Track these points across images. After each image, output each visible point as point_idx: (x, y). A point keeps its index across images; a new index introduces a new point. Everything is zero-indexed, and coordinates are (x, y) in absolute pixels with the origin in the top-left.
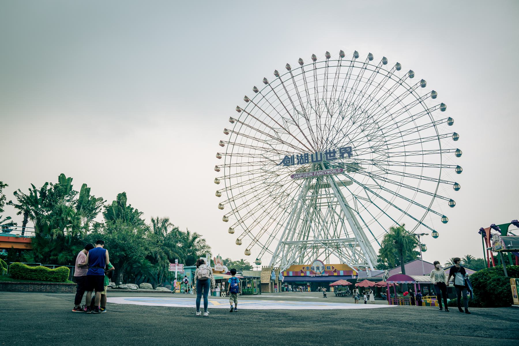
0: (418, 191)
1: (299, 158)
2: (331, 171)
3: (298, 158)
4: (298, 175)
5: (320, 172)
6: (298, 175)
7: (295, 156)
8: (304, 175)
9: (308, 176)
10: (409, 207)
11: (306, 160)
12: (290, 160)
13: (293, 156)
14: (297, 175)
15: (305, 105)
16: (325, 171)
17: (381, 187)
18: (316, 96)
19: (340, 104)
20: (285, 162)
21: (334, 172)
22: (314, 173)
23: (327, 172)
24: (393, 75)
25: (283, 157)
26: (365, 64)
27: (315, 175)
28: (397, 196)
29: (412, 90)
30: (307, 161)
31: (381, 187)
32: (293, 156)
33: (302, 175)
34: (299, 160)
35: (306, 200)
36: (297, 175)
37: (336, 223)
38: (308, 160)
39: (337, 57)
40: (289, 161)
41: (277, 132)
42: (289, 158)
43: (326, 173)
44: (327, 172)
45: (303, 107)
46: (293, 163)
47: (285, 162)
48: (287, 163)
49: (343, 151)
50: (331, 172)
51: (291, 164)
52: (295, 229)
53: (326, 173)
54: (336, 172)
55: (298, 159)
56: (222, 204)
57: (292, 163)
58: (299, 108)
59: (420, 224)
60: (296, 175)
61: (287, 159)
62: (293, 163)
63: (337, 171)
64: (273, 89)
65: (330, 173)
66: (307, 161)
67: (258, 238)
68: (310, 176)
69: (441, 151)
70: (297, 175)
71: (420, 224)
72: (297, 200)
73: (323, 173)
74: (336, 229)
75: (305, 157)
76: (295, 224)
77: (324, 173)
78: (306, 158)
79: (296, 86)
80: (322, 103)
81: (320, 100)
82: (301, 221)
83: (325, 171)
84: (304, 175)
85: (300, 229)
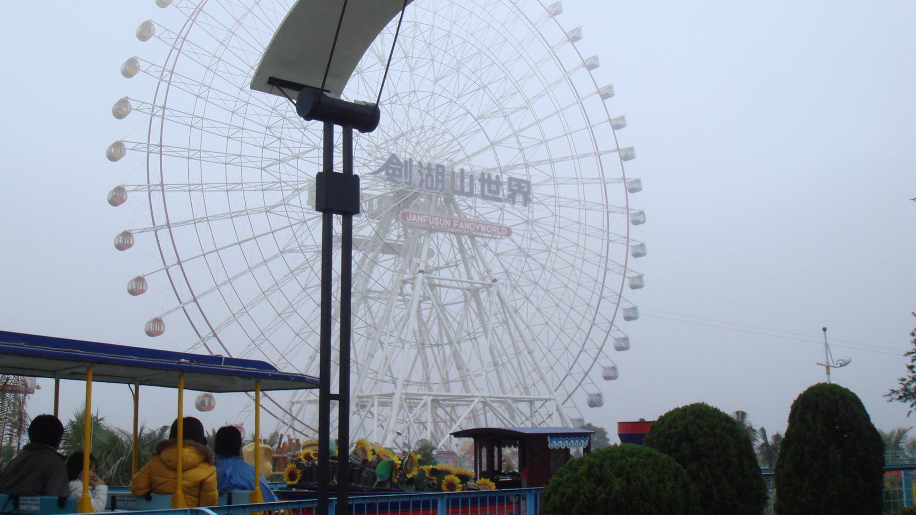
1: (425, 172)
3: (422, 170)
4: (466, 223)
5: (420, 215)
6: (419, 216)
7: (414, 163)
8: (431, 221)
12: (403, 169)
13: (411, 160)
14: (417, 215)
17: (287, 184)
18: (254, 189)
20: (391, 171)
21: (495, 230)
22: (455, 221)
24: (378, 136)
27: (457, 227)
30: (440, 187)
31: (287, 184)
32: (411, 160)
36: (415, 216)
40: (400, 170)
42: (399, 163)
46: (408, 180)
47: (391, 171)
48: (394, 174)
49: (514, 185)
51: (404, 180)
60: (413, 214)
61: (394, 164)
64: (280, 148)
65: (486, 230)
66: (440, 187)
68: (444, 226)
70: (415, 216)
73: (472, 227)
75: (438, 174)
77: (474, 228)
78: (440, 178)
80: (274, 173)
81: (267, 177)
84: (431, 221)
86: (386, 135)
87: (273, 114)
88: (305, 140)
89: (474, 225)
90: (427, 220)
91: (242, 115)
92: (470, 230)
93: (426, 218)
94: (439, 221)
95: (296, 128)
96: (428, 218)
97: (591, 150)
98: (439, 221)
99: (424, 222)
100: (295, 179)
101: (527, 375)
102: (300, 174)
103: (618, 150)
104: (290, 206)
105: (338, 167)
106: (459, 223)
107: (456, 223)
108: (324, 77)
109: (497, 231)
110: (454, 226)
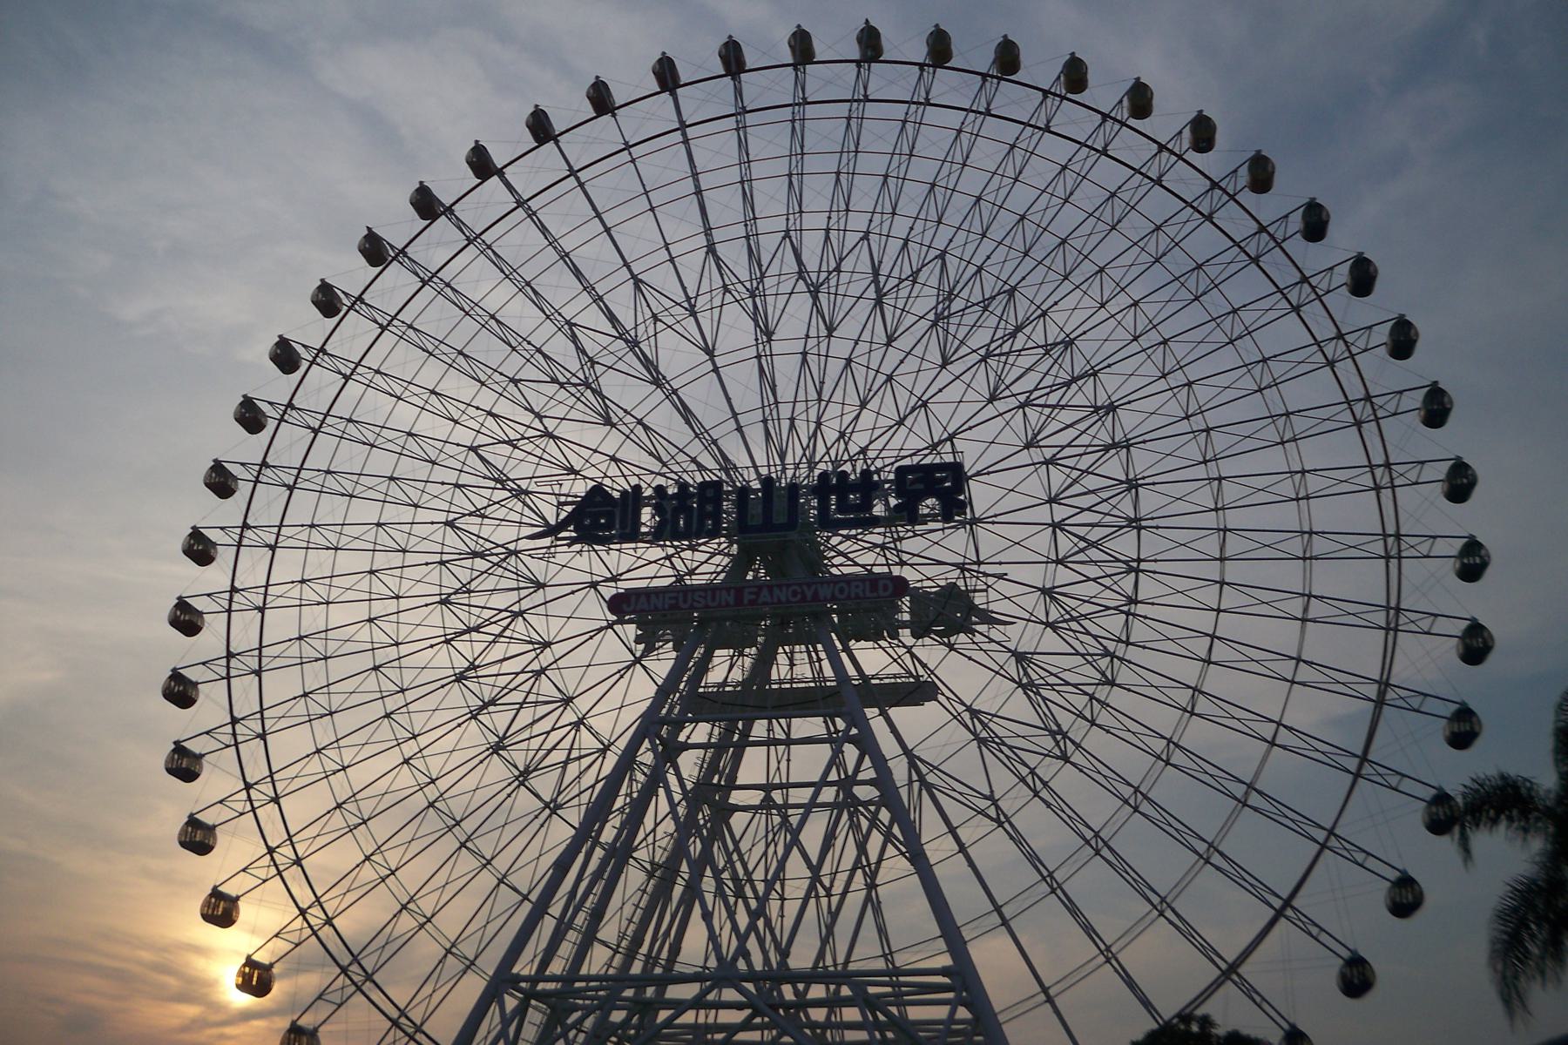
0: (1136, 809)
2: (838, 587)
3: (664, 503)
6: (653, 597)
8: (685, 601)
9: (707, 606)
10: (1185, 883)
11: (709, 516)
15: (768, 244)
16: (809, 585)
19: (1012, 320)
22: (747, 590)
23: (816, 589)
25: (581, 488)
26: (1109, 123)
27: (752, 603)
28: (1036, 794)
29: (1329, 349)
32: (637, 488)
33: (676, 598)
34: (668, 516)
35: (686, 746)
37: (835, 900)
38: (717, 515)
39: (984, 59)
41: (591, 359)
43: (809, 595)
44: (816, 589)
45: (753, 255)
49: (913, 482)
50: (842, 591)
52: (597, 915)
53: (809, 595)
54: (868, 594)
55: (658, 509)
56: (191, 746)
57: (623, 527)
58: (734, 255)
59: (1282, 1028)
62: (628, 531)
63: (872, 592)
67: (374, 957)
68: (720, 606)
69: (1327, 839)
71: (1282, 1028)
72: (1374, 698)
73: (795, 594)
74: (830, 929)
76: (598, 889)
77: (799, 596)
79: (748, 155)
82: (633, 878)
83: (809, 585)
84: (685, 601)
85: (624, 923)
86: (1062, 744)
87: (1034, 307)
88: (964, 350)
89: (799, 590)
90: (673, 602)
91: (1086, 285)
92: (788, 601)
93: (670, 598)
94: (705, 598)
95: (992, 341)
96: (676, 598)
97: (1328, 826)
98: (705, 598)
99: (666, 606)
100: (841, 290)
101: (594, 971)
102: (849, 302)
103: (449, 210)
104: (330, 990)
105: (1286, 1026)
106: (758, 594)
107: (751, 593)
108: (981, 871)
109: (864, 591)
110: (746, 602)
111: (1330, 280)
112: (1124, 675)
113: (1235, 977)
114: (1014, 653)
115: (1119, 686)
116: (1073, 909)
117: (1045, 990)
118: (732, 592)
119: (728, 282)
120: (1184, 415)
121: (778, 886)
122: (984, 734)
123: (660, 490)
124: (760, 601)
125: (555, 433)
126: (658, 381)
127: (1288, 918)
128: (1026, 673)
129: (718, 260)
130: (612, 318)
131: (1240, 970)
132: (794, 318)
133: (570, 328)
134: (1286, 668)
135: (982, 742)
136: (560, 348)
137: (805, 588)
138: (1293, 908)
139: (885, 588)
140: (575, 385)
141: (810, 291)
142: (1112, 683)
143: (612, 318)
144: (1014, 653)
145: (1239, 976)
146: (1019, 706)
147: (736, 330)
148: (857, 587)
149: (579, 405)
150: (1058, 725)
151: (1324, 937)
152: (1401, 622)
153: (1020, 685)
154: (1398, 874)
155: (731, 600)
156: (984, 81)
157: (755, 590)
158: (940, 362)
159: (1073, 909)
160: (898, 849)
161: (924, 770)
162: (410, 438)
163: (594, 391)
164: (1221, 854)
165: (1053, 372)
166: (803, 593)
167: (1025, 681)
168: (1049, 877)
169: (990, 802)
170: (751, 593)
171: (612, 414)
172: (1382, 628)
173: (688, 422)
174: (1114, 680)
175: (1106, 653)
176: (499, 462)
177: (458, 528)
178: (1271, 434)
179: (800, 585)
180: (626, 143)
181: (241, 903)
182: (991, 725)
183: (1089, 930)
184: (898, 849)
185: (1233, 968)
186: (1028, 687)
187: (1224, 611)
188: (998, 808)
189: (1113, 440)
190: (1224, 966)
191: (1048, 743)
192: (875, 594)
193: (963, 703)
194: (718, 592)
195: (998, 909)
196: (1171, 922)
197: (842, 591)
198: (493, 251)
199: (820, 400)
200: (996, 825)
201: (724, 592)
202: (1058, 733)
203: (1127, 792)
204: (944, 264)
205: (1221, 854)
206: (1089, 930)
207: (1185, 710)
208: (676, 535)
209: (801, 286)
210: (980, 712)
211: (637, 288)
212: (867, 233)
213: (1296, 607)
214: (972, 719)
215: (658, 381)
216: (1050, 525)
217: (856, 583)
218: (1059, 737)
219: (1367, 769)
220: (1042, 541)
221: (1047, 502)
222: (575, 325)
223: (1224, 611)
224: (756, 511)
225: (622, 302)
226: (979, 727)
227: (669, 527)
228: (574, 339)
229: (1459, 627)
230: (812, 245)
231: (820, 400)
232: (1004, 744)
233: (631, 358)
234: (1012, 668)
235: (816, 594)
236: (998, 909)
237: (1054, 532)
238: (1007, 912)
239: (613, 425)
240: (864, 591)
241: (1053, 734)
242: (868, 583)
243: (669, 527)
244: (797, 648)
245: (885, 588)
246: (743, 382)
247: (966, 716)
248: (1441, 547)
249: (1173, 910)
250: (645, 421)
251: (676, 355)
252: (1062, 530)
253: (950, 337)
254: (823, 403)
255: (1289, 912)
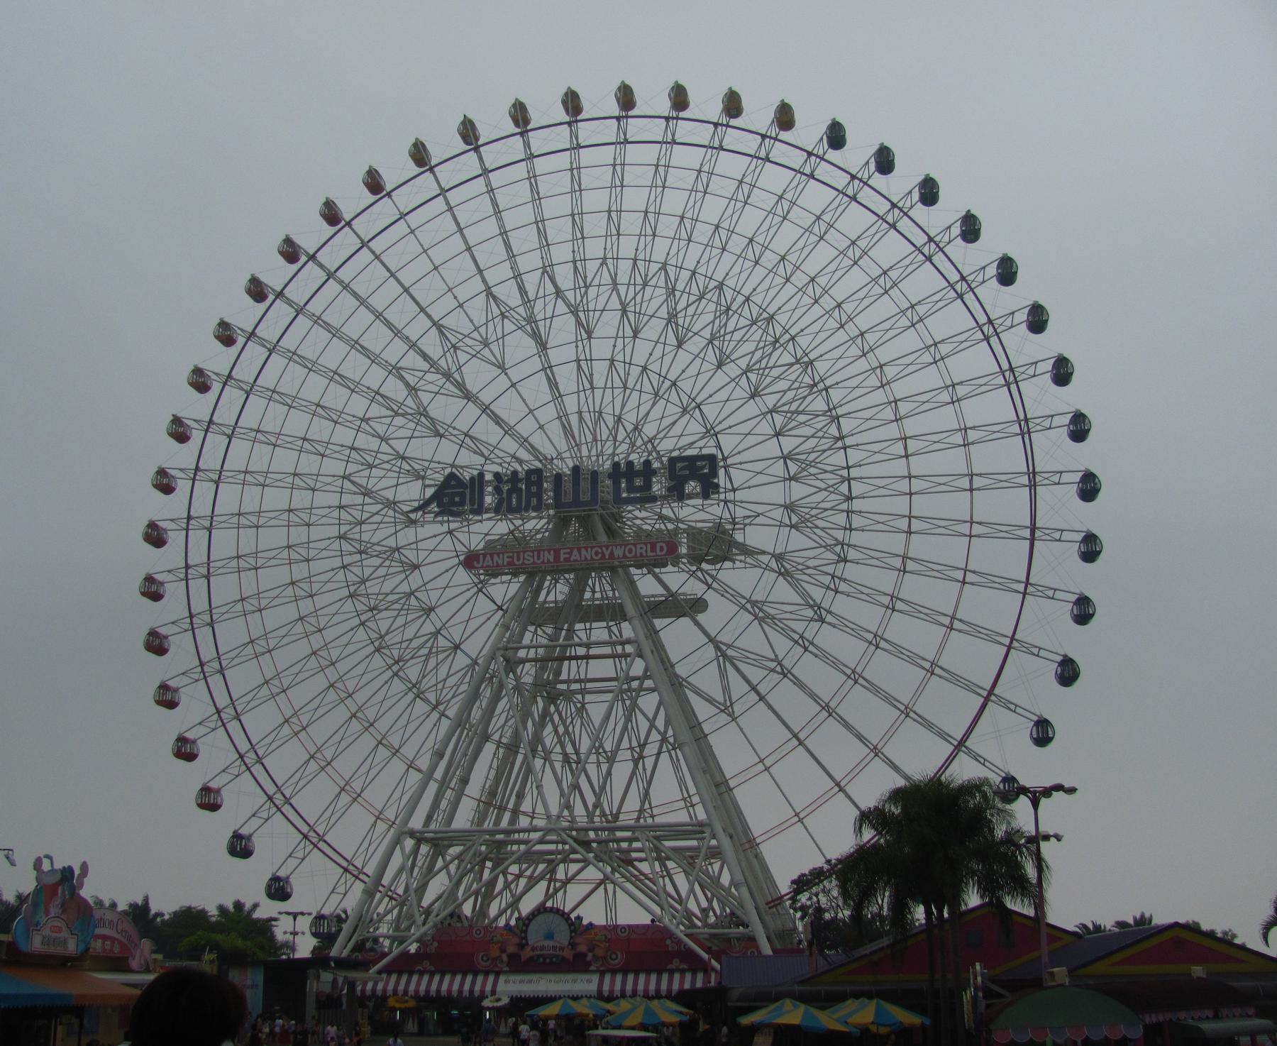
15: (531, 282)
16: (607, 547)
22: (562, 552)
34: (505, 495)
43: (607, 554)
44: (612, 550)
50: (630, 551)
53: (607, 554)
54: (649, 554)
63: (651, 551)
73: (597, 554)
77: (600, 555)
83: (607, 547)
89: (600, 551)
92: (592, 559)
106: (570, 554)
107: (565, 553)
109: (646, 551)
110: (562, 559)
111: (372, 573)
112: (852, 554)
113: (963, 749)
114: (773, 555)
115: (850, 561)
116: (847, 726)
117: (838, 784)
118: (552, 552)
119: (503, 310)
120: (861, 354)
121: (636, 755)
122: (761, 614)
123: (497, 476)
124: (572, 559)
125: (406, 455)
126: (468, 396)
127: (993, 701)
128: (782, 566)
129: (495, 298)
130: (425, 356)
131: (967, 744)
132: (562, 330)
133: (395, 371)
134: (965, 528)
135: (761, 620)
136: (395, 389)
137: (604, 548)
138: (995, 695)
139: (662, 549)
140: (411, 415)
141: (572, 312)
142: (845, 561)
143: (425, 356)
144: (773, 555)
145: (966, 747)
146: (783, 591)
147: (519, 346)
148: (641, 548)
149: (419, 428)
150: (814, 601)
151: (1018, 710)
152: (1037, 480)
153: (780, 574)
154: (1062, 658)
155: (552, 559)
156: (668, 122)
157: (569, 550)
158: (676, 344)
159: (847, 726)
160: (719, 708)
161: (724, 648)
162: (296, 477)
163: (425, 416)
164: (941, 668)
165: (764, 339)
166: (603, 553)
167: (783, 570)
168: (826, 707)
169: (776, 664)
170: (565, 553)
171: (439, 428)
172: (1027, 486)
173: (497, 423)
174: (846, 558)
175: (838, 543)
176: (363, 482)
177: (349, 539)
178: (927, 358)
179: (601, 547)
180: (401, 213)
181: (254, 838)
182: (764, 608)
183: (860, 737)
184: (719, 708)
185: (962, 743)
186: (784, 574)
187: (915, 493)
188: (781, 666)
189: (814, 381)
190: (956, 743)
191: (810, 613)
192: (654, 554)
193: (744, 597)
194: (542, 553)
195: (795, 736)
196: (915, 720)
197: (630, 551)
198: (322, 321)
199: (625, 387)
200: (782, 676)
201: (546, 552)
202: (816, 607)
203: (843, 587)
204: (666, 272)
205: (941, 668)
206: (860, 737)
207: (900, 570)
208: (511, 510)
209: (561, 307)
210: (757, 602)
211: (441, 333)
212: (605, 259)
213: (965, 483)
214: (752, 608)
215: (468, 396)
216: (781, 458)
217: (642, 545)
218: (816, 608)
219: (1030, 589)
220: (779, 468)
221: (774, 436)
222: (400, 368)
223: (915, 493)
224: (568, 486)
225: (432, 345)
226: (757, 610)
227: (505, 504)
228: (401, 378)
229: (1077, 477)
230: (565, 277)
231: (625, 387)
232: (775, 618)
233: (448, 385)
234: (774, 565)
235: (612, 554)
236: (795, 736)
237: (785, 463)
238: (802, 736)
239: (441, 436)
240: (646, 551)
241: (812, 607)
242: (649, 546)
243: (505, 504)
244: (595, 625)
245: (662, 549)
246: (537, 389)
247: (748, 606)
248: (1058, 421)
249: (915, 712)
250: (470, 433)
251: (477, 375)
252: (791, 459)
253: (680, 328)
254: (628, 391)
255: (993, 698)
